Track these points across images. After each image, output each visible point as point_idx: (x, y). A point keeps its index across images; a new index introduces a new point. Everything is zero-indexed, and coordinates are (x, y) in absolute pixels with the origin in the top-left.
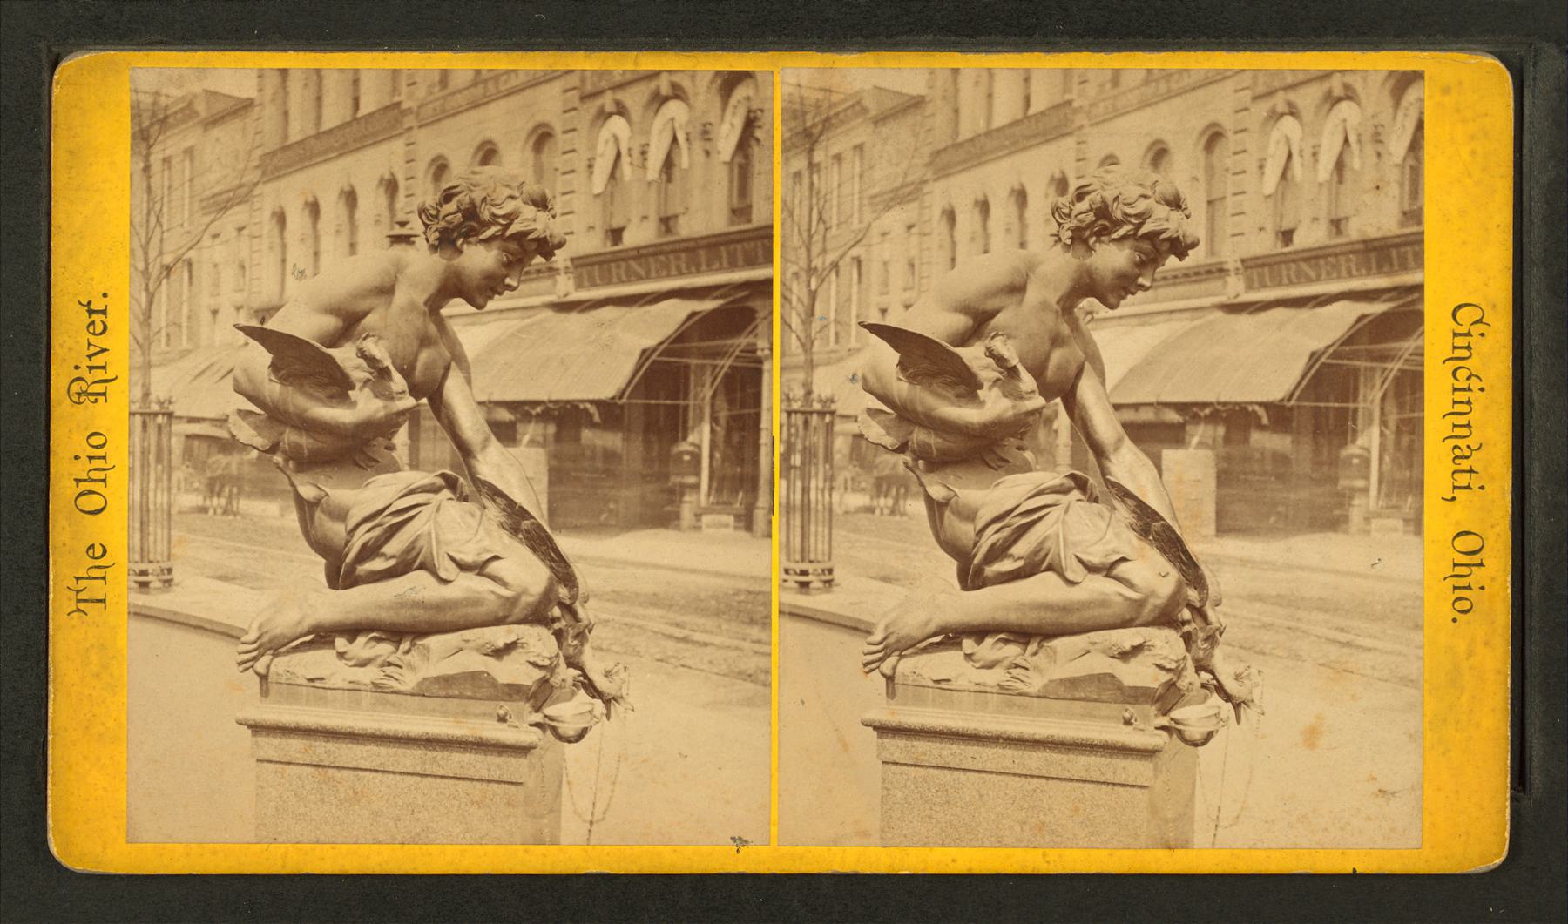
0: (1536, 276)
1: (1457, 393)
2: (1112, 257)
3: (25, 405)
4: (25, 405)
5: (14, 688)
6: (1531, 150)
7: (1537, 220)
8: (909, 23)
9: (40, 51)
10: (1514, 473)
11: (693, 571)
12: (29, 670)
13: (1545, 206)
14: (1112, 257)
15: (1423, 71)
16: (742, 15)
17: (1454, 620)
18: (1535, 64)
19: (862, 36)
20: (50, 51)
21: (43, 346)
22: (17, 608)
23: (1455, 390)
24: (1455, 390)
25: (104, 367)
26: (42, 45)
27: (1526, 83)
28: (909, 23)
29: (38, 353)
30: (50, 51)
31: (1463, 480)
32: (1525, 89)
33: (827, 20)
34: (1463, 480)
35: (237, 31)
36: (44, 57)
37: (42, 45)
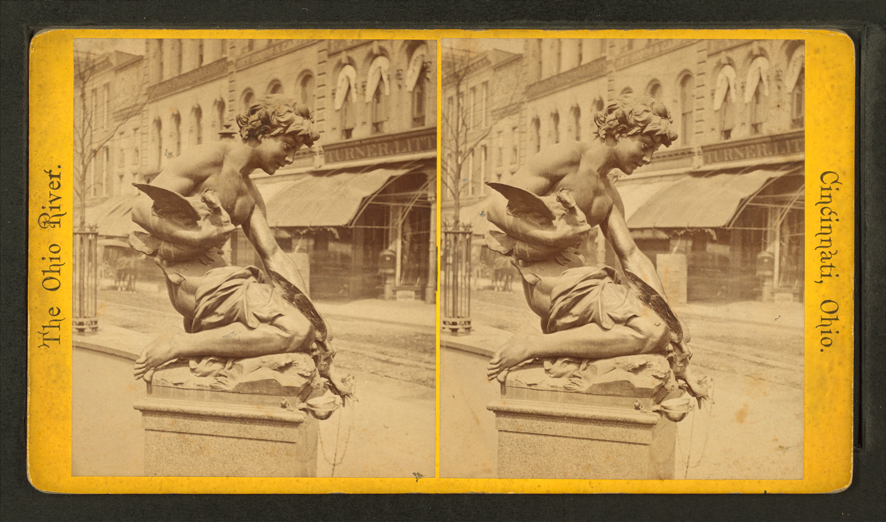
0: (868, 156)
1: (823, 222)
2: (628, 145)
3: (14, 229)
4: (14, 229)
5: (8, 389)
6: (865, 85)
7: (868, 124)
8: (514, 13)
9: (23, 29)
10: (855, 267)
11: (392, 323)
12: (17, 378)
13: (873, 116)
14: (628, 145)
15: (804, 40)
16: (419, 8)
17: (822, 350)
18: (867, 36)
19: (487, 20)
20: (28, 29)
21: (24, 195)
22: (10, 343)
23: (822, 220)
24: (822, 220)
25: (59, 208)
26: (24, 26)
27: (862, 47)
28: (514, 13)
29: (22, 199)
30: (28, 29)
31: (827, 271)
32: (862, 50)
33: (467, 11)
34: (827, 271)
35: (134, 17)
36: (25, 32)
37: (24, 26)
